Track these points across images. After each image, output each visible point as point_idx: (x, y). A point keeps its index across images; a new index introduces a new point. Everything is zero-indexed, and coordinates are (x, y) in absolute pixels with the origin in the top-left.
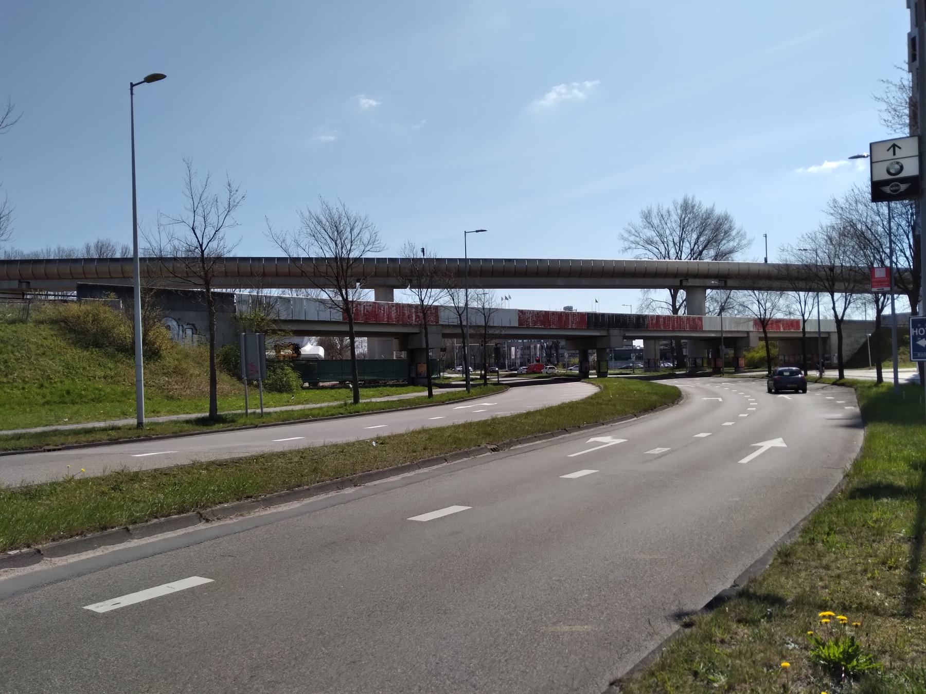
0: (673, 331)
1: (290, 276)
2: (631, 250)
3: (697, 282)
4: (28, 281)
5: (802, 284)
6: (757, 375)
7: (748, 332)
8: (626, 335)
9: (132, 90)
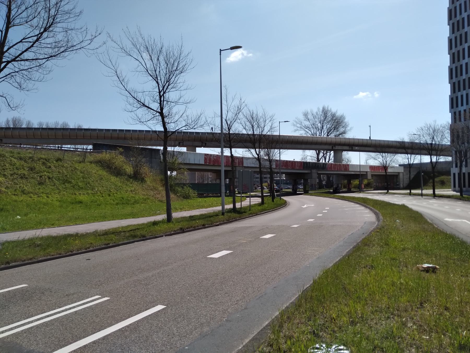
0: (337, 171)
1: (118, 139)
2: (298, 131)
3: (340, 148)
4: (1, 139)
5: (409, 151)
6: (383, 192)
7: (367, 172)
8: (318, 172)
9: (220, 52)
